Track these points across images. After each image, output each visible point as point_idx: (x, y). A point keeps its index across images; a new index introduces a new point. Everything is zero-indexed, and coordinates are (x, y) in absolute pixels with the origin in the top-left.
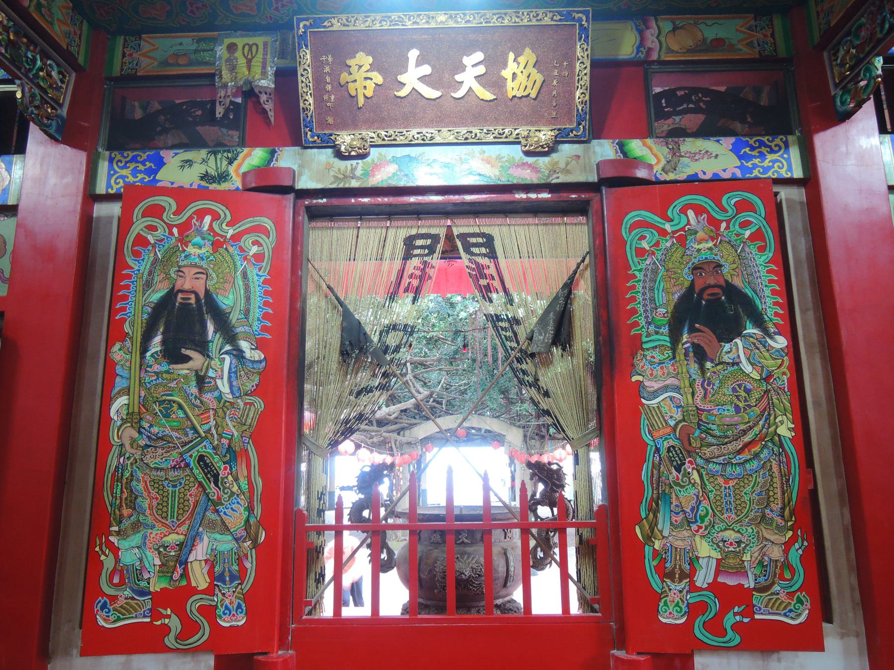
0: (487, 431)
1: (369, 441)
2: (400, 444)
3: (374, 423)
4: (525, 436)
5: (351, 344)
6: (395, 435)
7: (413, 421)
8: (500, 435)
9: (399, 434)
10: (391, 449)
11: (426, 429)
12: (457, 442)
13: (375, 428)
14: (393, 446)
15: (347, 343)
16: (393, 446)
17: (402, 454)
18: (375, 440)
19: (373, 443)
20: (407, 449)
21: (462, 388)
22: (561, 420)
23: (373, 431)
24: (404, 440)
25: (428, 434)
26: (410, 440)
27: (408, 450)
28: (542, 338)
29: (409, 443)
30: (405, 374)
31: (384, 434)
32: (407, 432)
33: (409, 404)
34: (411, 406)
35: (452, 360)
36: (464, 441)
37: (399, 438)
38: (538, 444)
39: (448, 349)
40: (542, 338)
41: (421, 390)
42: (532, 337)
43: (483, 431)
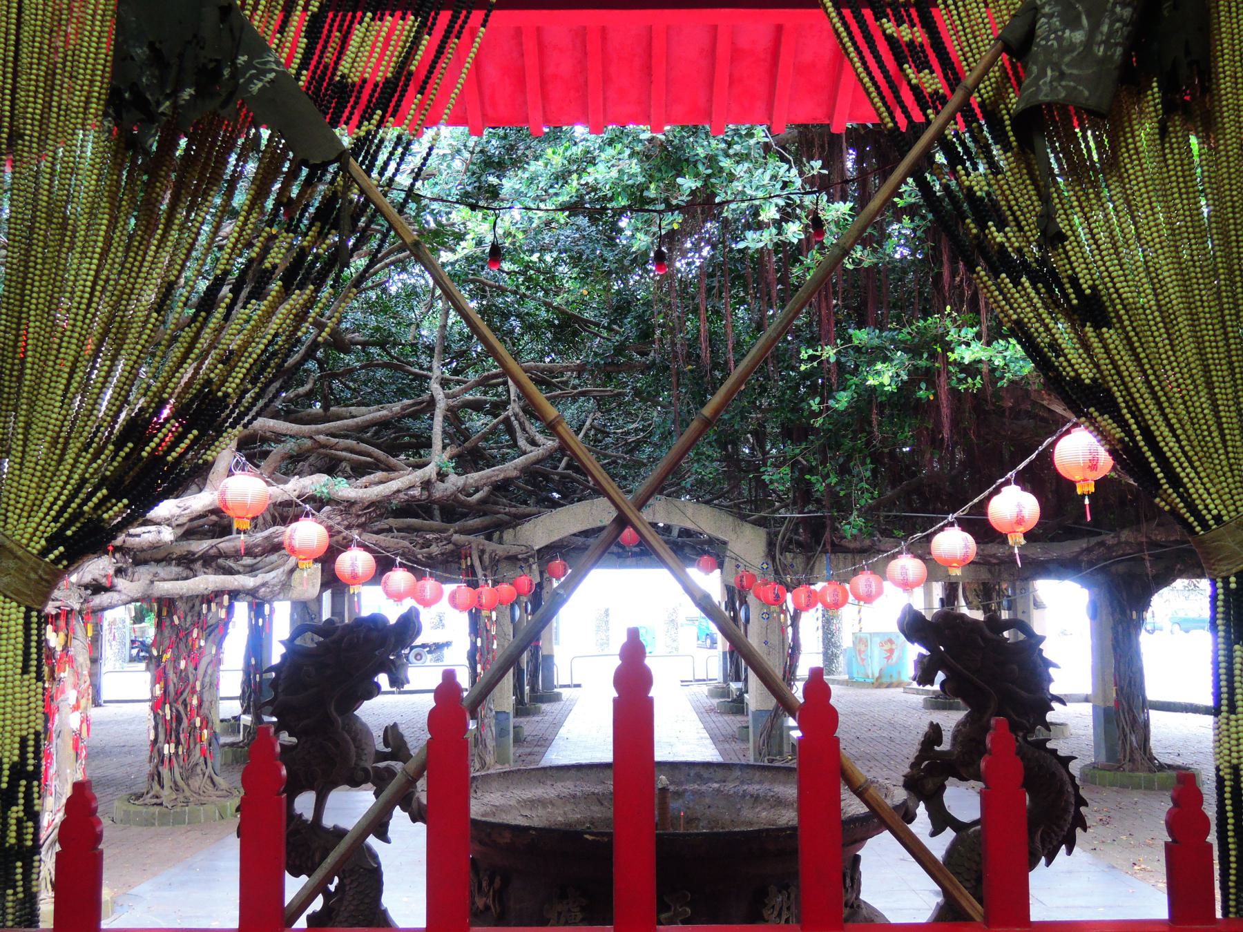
0: (685, 533)
1: (421, 554)
2: (492, 559)
3: (437, 513)
4: (771, 545)
5: (157, 58)
6: (481, 539)
7: (523, 509)
8: (711, 541)
9: (489, 538)
10: (471, 571)
11: (545, 529)
12: (619, 556)
13: (436, 523)
14: (477, 564)
15: (141, 52)
16: (477, 564)
17: (495, 583)
18: (435, 550)
19: (430, 557)
20: (506, 571)
21: (631, 439)
22: (1161, 430)
23: (432, 531)
24: (500, 550)
25: (555, 538)
26: (514, 550)
27: (509, 574)
28: (1079, 36)
29: (512, 559)
30: (504, 405)
31: (456, 537)
32: (508, 535)
33: (510, 469)
34: (515, 473)
35: (609, 369)
36: (634, 555)
37: (491, 546)
38: (799, 562)
39: (597, 344)
40: (1079, 36)
41: (539, 438)
42: (1030, 35)
43: (675, 533)
